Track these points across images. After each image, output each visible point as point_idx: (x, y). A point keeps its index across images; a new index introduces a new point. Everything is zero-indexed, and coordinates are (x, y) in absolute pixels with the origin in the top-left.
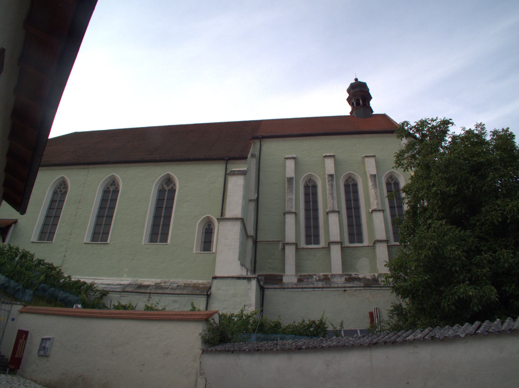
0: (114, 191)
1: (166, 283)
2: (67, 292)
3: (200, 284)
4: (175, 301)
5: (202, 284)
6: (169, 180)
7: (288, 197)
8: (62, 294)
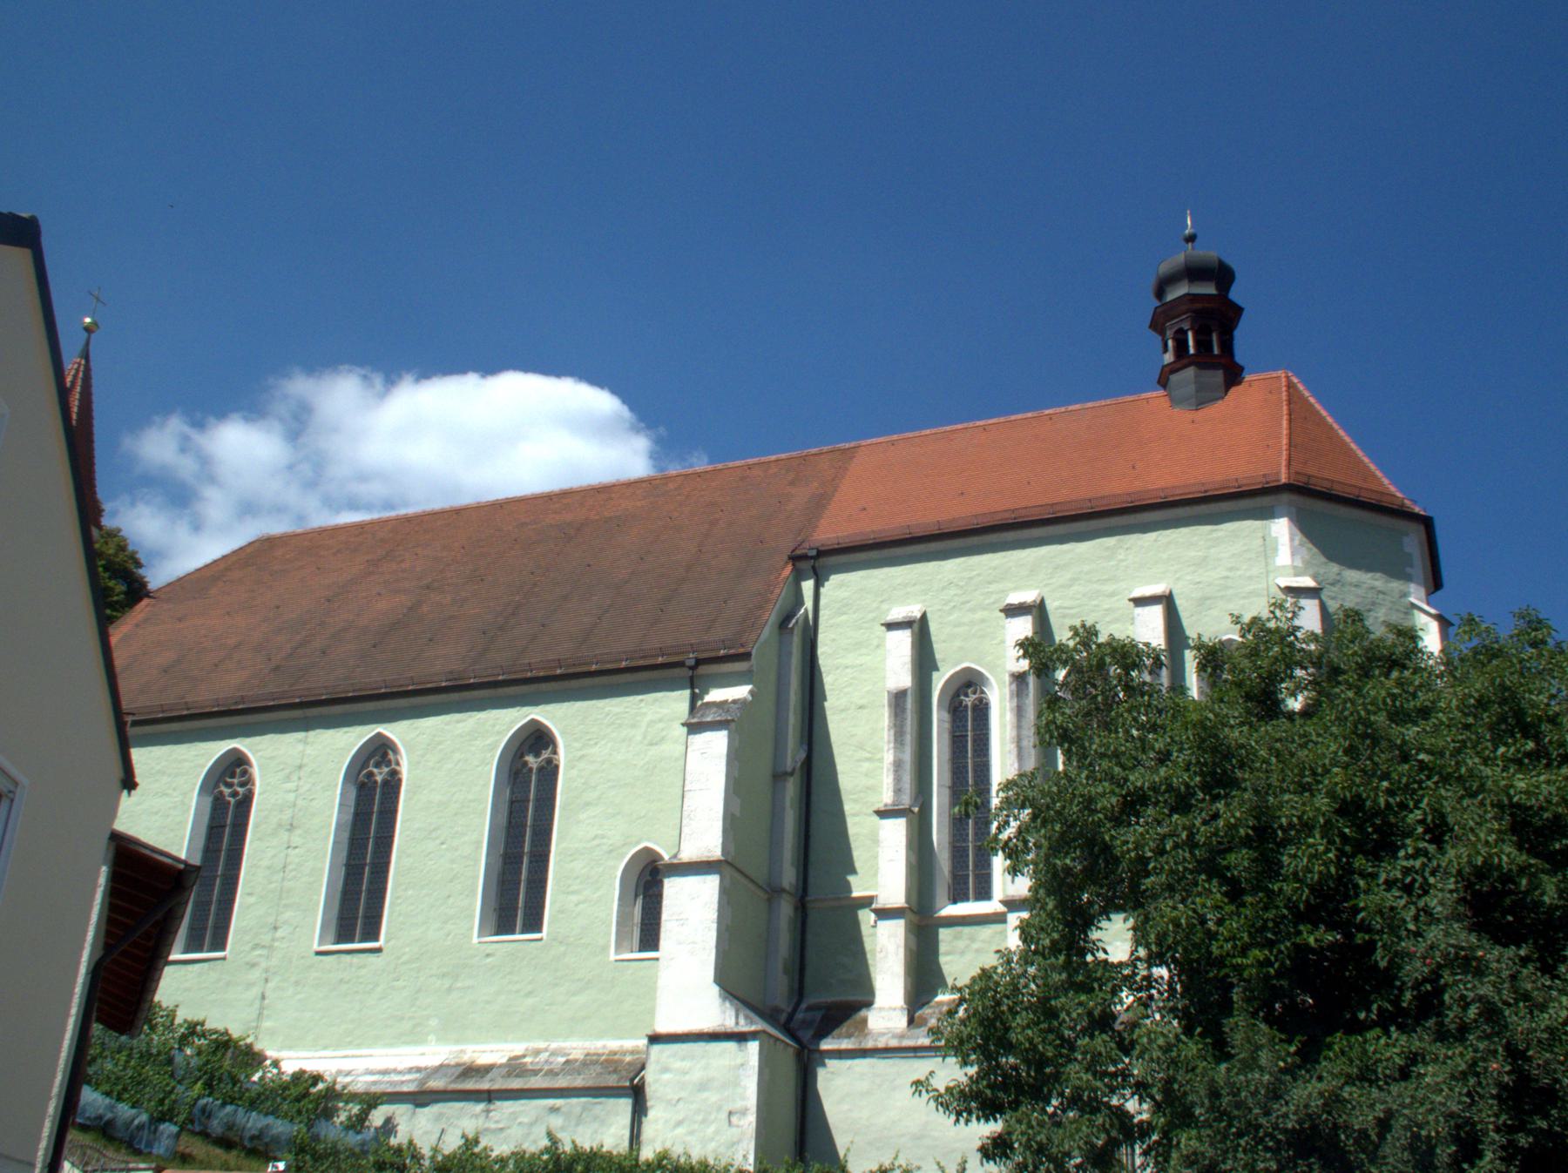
0: (385, 783)
1: (537, 1052)
2: (267, 1114)
3: (624, 1053)
4: (554, 1110)
5: (632, 1052)
8: (254, 1122)
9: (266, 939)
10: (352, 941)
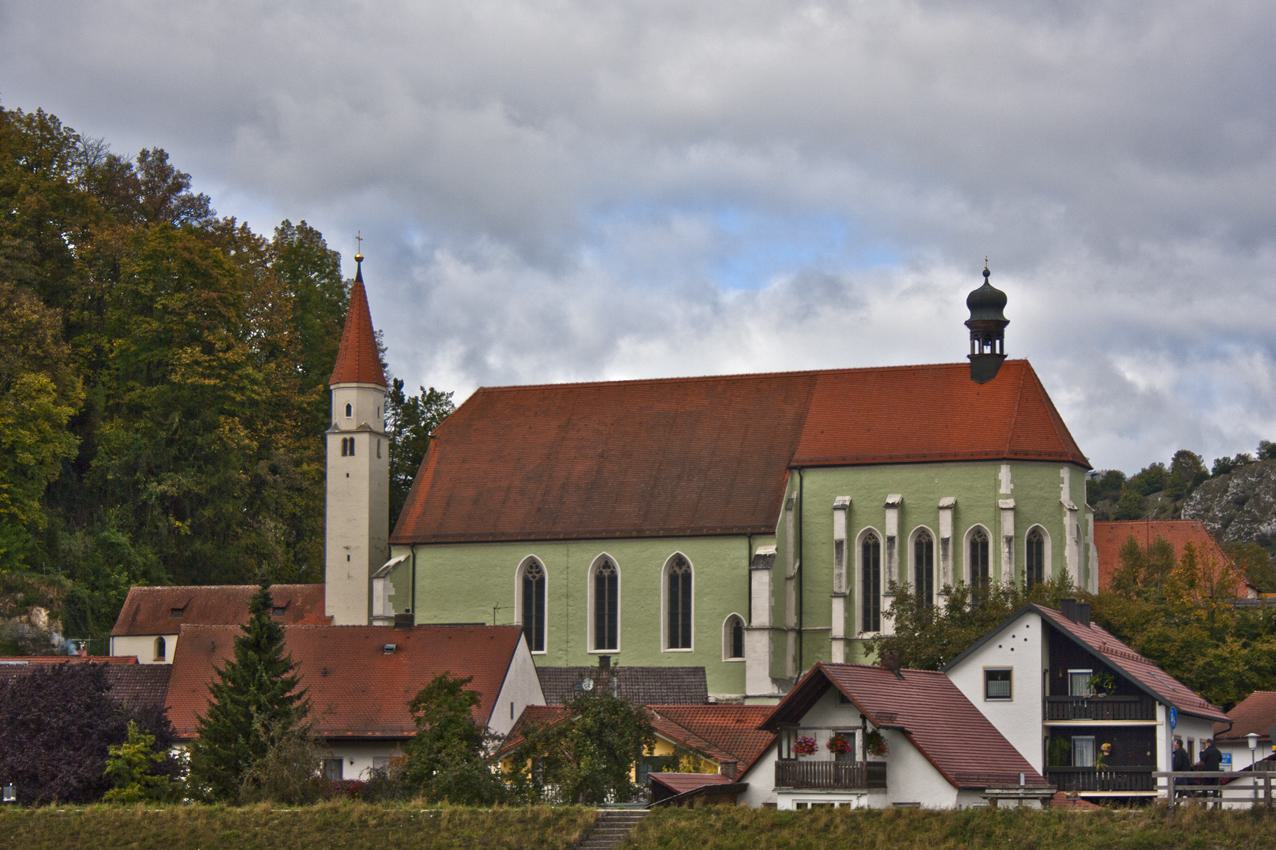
0: (609, 577)
3: (732, 700)
5: (736, 700)
6: (679, 561)
7: (836, 571)
9: (564, 646)
10: (604, 648)
